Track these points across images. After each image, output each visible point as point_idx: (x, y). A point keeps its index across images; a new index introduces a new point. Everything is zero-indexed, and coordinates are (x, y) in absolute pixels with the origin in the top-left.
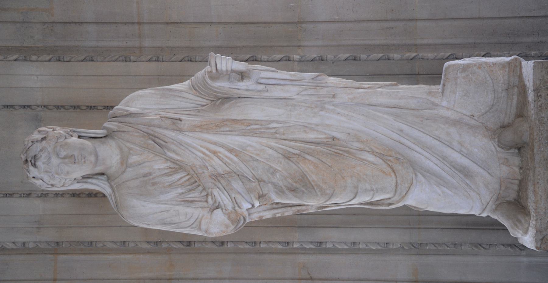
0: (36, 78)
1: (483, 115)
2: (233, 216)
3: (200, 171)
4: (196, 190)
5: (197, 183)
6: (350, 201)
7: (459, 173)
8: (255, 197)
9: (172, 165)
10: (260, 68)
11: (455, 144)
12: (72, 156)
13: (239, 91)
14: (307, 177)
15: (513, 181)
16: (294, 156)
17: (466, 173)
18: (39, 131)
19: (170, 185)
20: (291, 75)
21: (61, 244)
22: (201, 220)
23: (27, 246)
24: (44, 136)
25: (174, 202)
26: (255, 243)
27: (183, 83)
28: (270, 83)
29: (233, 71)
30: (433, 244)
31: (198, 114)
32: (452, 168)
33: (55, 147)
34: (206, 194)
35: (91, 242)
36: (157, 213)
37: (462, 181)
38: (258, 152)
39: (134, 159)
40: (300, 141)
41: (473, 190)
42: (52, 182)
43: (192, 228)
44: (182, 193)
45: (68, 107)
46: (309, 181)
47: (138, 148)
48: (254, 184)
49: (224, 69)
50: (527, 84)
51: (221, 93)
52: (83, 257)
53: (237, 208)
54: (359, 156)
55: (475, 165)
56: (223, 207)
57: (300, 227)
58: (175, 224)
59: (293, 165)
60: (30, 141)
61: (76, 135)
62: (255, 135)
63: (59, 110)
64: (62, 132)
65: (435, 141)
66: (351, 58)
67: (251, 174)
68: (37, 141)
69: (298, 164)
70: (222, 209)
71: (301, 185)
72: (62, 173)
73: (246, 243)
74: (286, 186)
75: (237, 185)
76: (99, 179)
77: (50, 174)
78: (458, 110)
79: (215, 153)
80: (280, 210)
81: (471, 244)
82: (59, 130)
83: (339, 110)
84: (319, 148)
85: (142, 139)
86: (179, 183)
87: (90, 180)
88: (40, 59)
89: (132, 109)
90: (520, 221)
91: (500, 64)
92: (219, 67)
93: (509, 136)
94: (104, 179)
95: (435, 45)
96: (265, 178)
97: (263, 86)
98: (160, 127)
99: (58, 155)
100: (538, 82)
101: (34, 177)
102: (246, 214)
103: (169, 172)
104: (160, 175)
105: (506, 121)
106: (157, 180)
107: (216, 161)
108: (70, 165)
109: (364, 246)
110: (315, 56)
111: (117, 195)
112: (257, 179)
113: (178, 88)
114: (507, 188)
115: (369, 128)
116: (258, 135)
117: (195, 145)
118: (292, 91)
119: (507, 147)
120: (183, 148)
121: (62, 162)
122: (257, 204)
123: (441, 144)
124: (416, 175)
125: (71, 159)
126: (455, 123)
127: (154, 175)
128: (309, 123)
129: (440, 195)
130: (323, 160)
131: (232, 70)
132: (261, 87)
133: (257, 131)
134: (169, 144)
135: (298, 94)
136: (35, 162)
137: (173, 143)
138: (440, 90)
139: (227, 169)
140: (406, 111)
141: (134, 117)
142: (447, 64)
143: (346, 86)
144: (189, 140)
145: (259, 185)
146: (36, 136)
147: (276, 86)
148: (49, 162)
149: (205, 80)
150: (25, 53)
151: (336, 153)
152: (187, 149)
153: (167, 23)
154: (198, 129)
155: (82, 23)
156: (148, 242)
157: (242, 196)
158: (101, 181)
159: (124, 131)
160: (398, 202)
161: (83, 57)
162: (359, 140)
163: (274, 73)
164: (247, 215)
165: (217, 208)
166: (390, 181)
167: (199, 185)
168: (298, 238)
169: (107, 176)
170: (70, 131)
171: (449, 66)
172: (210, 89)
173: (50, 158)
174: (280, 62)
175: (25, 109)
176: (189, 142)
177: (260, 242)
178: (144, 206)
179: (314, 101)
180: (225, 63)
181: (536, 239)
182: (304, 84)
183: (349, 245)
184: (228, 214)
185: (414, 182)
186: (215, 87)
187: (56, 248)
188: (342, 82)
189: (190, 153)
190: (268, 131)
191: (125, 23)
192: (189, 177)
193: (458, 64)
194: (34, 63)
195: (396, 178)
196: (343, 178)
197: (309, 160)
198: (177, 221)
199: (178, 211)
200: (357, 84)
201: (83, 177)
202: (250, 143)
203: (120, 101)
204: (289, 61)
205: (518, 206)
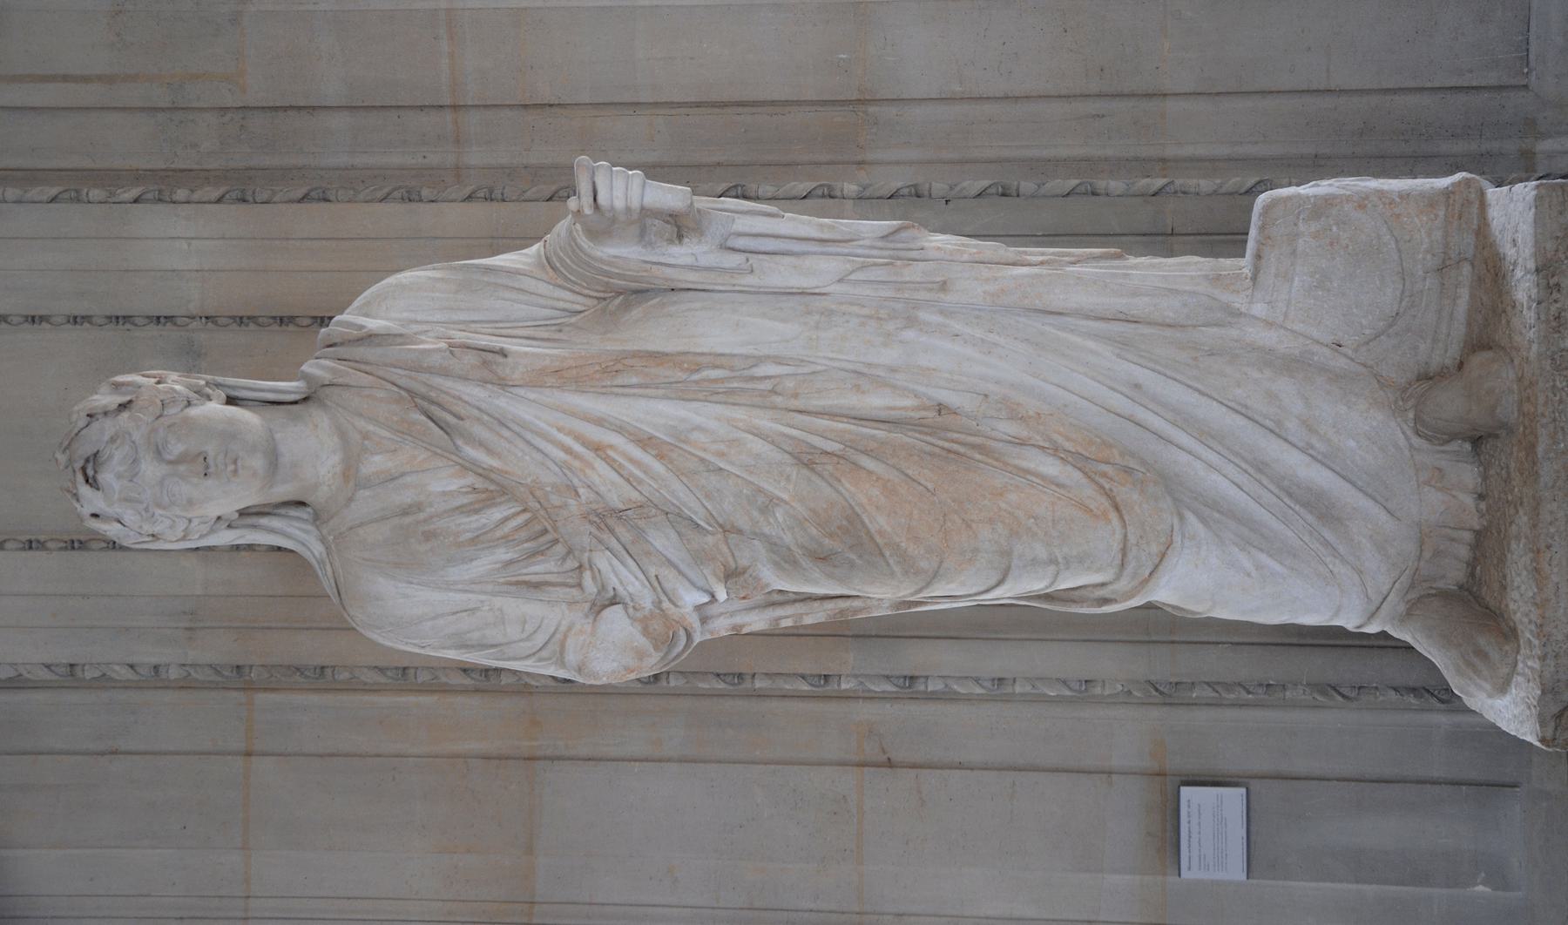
0: (185, 246)
1: (1367, 343)
2: (657, 626)
3: (556, 500)
5: (550, 535)
6: (987, 591)
7: (1302, 511)
8: (715, 575)
9: (480, 483)
11: (1292, 425)
13: (668, 271)
14: (863, 523)
15: (1455, 534)
16: (825, 459)
17: (1321, 508)
19: (473, 540)
20: (821, 226)
22: (565, 637)
25: (490, 587)
26: (740, 676)
28: (763, 249)
29: (646, 212)
30: (1208, 684)
31: (557, 336)
32: (1282, 495)
36: (442, 615)
37: (1311, 534)
38: (722, 447)
39: (376, 463)
41: (1344, 561)
42: (148, 528)
43: (540, 660)
44: (511, 562)
46: (868, 532)
47: (387, 434)
48: (710, 539)
49: (619, 204)
50: (1510, 252)
52: (315, 699)
53: (666, 604)
54: (1016, 462)
55: (1348, 486)
56: (628, 600)
58: (493, 646)
60: (83, 414)
62: (715, 398)
64: (178, 387)
65: (1235, 416)
66: (993, 190)
67: (702, 511)
68: (106, 413)
69: (835, 483)
70: (625, 604)
71: (846, 542)
74: (803, 547)
75: (663, 540)
78: (1298, 327)
79: (598, 449)
80: (789, 610)
81: (1308, 684)
82: (176, 382)
83: (957, 326)
84: (898, 437)
86: (499, 533)
87: (264, 521)
88: (196, 196)
89: (373, 324)
90: (1482, 654)
91: (1422, 195)
93: (1450, 404)
95: (1213, 160)
96: (742, 522)
98: (445, 373)
99: (158, 453)
100: (1550, 245)
101: (95, 515)
102: (694, 620)
105: (1436, 361)
107: (601, 474)
108: (195, 480)
109: (1028, 689)
110: (899, 184)
114: (1437, 553)
115: (1044, 380)
117: (543, 425)
118: (822, 271)
119: (1438, 435)
120: (506, 433)
121: (184, 475)
122: (722, 595)
123: (1250, 424)
124: (1181, 517)
125: (203, 466)
126: (1291, 365)
129: (1249, 575)
130: (910, 472)
131: (643, 208)
132: (734, 260)
133: (720, 387)
134: (467, 424)
135: (840, 281)
138: (1247, 271)
140: (1146, 330)
141: (379, 345)
142: (1262, 199)
143: (977, 258)
144: (525, 413)
146: (105, 399)
147: (778, 258)
149: (574, 240)
150: (161, 185)
151: (949, 451)
152: (518, 435)
153: (525, 106)
154: (551, 380)
155: (314, 108)
156: (465, 670)
157: (680, 572)
160: (1130, 595)
161: (303, 191)
162: (1015, 415)
164: (697, 625)
165: (614, 601)
166: (1106, 537)
167: (556, 541)
168: (849, 663)
170: (208, 384)
171: (1274, 203)
173: (135, 461)
176: (527, 417)
178: (406, 596)
179: (887, 299)
180: (622, 188)
181: (1540, 715)
182: (859, 251)
183: (988, 684)
185: (1177, 538)
186: (601, 261)
187: (238, 677)
188: (967, 246)
190: (750, 386)
191: (422, 108)
192: (527, 516)
193: (1299, 196)
194: (180, 207)
195: (1124, 526)
196: (969, 526)
197: (870, 473)
199: (500, 610)
200: (1011, 252)
201: (243, 513)
202: (698, 420)
203: (349, 303)
205: (1471, 601)
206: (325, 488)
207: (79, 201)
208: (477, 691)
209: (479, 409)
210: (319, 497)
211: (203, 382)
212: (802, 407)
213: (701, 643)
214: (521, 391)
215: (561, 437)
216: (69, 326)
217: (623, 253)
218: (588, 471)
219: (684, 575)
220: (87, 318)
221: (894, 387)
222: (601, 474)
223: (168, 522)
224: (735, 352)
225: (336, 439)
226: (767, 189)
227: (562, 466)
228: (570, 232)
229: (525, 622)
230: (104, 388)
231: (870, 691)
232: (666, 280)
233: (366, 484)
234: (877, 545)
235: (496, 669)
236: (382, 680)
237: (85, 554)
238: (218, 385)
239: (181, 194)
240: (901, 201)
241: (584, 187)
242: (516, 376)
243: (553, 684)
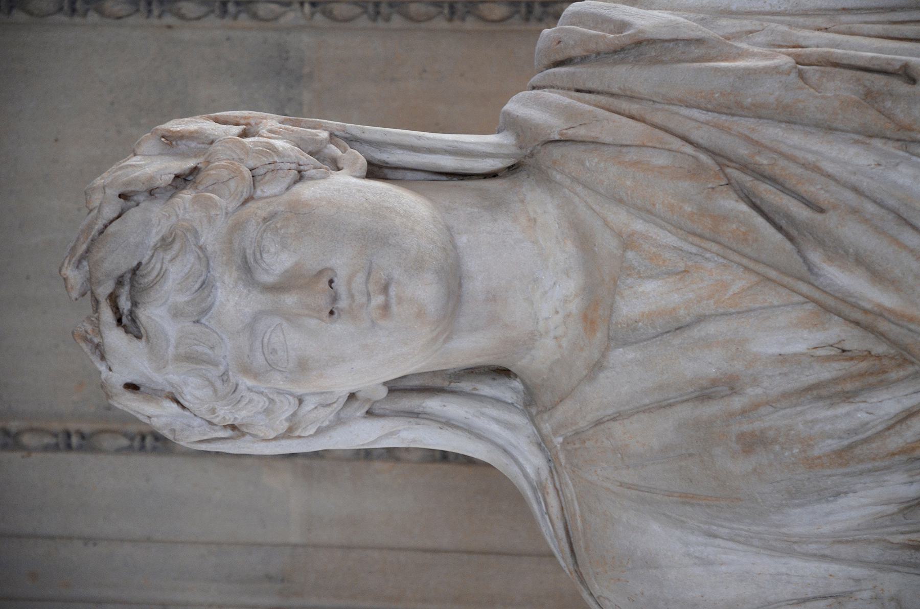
9: (855, 341)
12: (321, 273)
18: (171, 141)
24: (191, 163)
33: (238, 227)
42: (225, 414)
47: (670, 239)
60: (113, 193)
61: (358, 158)
63: (381, 24)
64: (279, 144)
68: (152, 193)
72: (272, 367)
76: (482, 398)
77: (214, 373)
82: (276, 135)
85: (685, 185)
86: (895, 442)
87: (433, 404)
98: (789, 117)
99: (247, 270)
101: (132, 387)
103: (835, 381)
104: (785, 395)
106: (770, 421)
108: (313, 323)
111: (570, 492)
125: (324, 294)
127: (753, 392)
134: (831, 221)
136: (135, 304)
141: (656, 61)
146: (150, 165)
148: (200, 310)
159: (595, 143)
169: (523, 383)
170: (333, 137)
173: (206, 285)
201: (395, 388)
206: (549, 342)
209: (855, 190)
210: (538, 360)
211: (324, 135)
216: (62, 18)
223: (262, 403)
230: (149, 144)
237: (90, 458)
238: (352, 141)
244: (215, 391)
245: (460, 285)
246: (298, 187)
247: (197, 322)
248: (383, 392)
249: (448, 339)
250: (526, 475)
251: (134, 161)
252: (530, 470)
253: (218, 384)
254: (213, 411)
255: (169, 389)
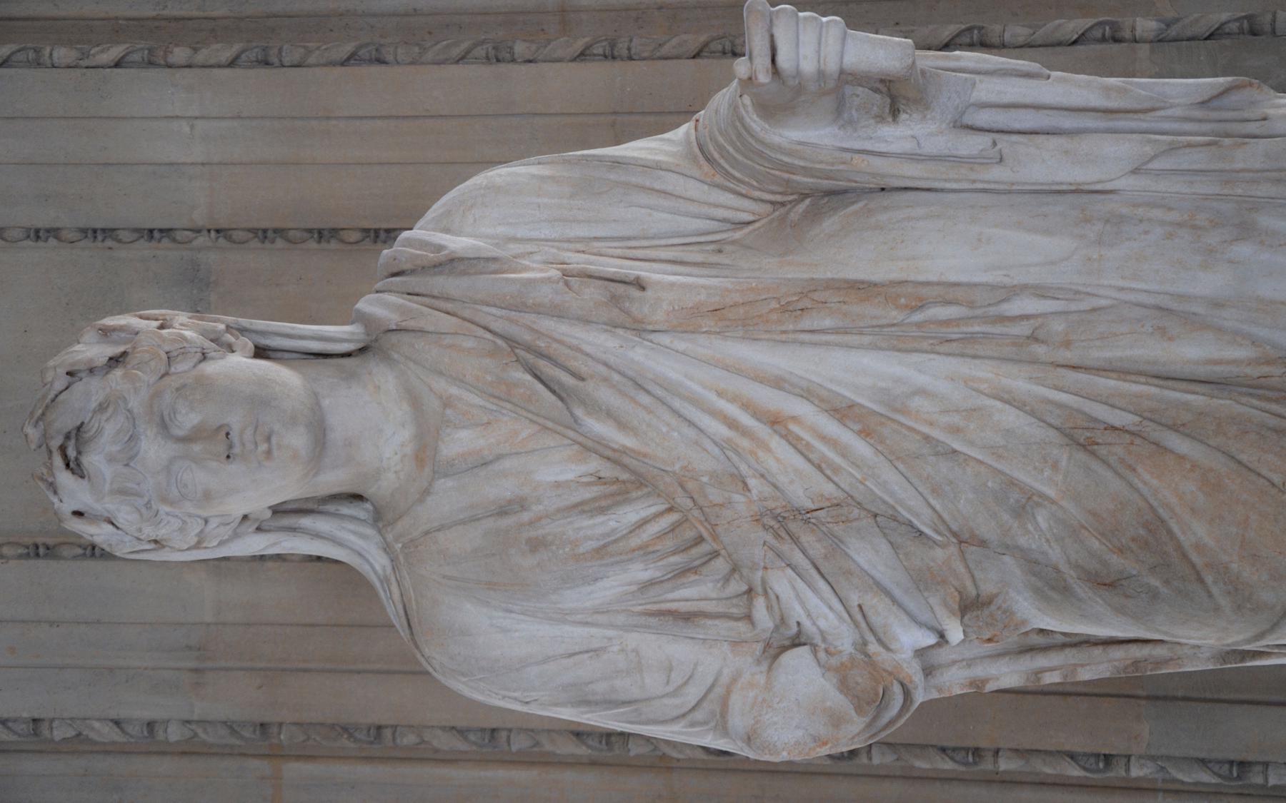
0: (187, 129)
2: (860, 678)
3: (715, 495)
4: (705, 570)
8: (945, 604)
9: (608, 471)
10: (971, 65)
12: (220, 427)
13: (877, 162)
16: (1110, 437)
18: (106, 332)
20: (1107, 89)
21: (275, 730)
22: (728, 692)
23: (160, 735)
24: (121, 349)
25: (620, 619)
26: (977, 752)
27: (666, 136)
28: (1017, 126)
29: (847, 78)
33: (157, 395)
34: (745, 588)
35: (379, 728)
38: (956, 419)
39: (460, 442)
40: (1140, 373)
42: (149, 531)
43: (692, 725)
44: (651, 583)
45: (298, 234)
46: (1179, 547)
47: (478, 400)
48: (939, 553)
49: (808, 67)
51: (806, 171)
52: (365, 771)
53: (874, 647)
56: (818, 640)
57: (1157, 698)
58: (629, 703)
59: (1109, 474)
60: (62, 371)
63: (267, 245)
67: (927, 512)
68: (91, 371)
73: (943, 750)
74: (1077, 567)
75: (870, 554)
76: (342, 517)
79: (776, 422)
80: (1055, 659)
82: (186, 327)
86: (635, 541)
87: (306, 522)
88: (200, 57)
89: (457, 243)
92: (784, 60)
94: (362, 515)
96: (986, 529)
97: (986, 140)
98: (559, 313)
99: (164, 426)
101: (78, 514)
103: (595, 499)
104: (558, 510)
107: (781, 458)
108: (214, 464)
110: (1224, 16)
111: (407, 583)
112: (955, 534)
113: (635, 154)
116: (954, 347)
120: (645, 399)
122: (955, 633)
125: (220, 442)
127: (537, 509)
128: (1181, 297)
130: (1244, 457)
131: (842, 72)
132: (974, 144)
133: (953, 332)
134: (590, 386)
136: (79, 453)
137: (606, 380)
139: (829, 489)
141: (464, 273)
145: (964, 559)
146: (91, 350)
148: (128, 455)
149: (741, 120)
157: (894, 601)
158: (351, 526)
159: (422, 331)
161: (349, 48)
163: (1033, 83)
164: (918, 678)
165: (796, 642)
167: (715, 554)
170: (229, 328)
172: (760, 154)
174: (1079, 47)
175: (154, 244)
177: (997, 752)
179: (1206, 197)
180: (816, 44)
182: (1166, 126)
184: (837, 670)
186: (779, 149)
189: (674, 421)
190: (998, 329)
192: (674, 517)
194: (179, 74)
197: (1182, 458)
198: (636, 693)
199: (636, 651)
201: (278, 511)
202: (922, 380)
204: (1116, 40)
207: (39, 64)
208: (593, 763)
209: (606, 364)
211: (222, 327)
212: (1075, 361)
213: (922, 704)
214: (665, 339)
215: (723, 405)
217: (812, 137)
218: (761, 454)
219: (900, 606)
220: (54, 232)
221: (1219, 330)
222: (781, 458)
223: (176, 524)
224: (976, 279)
225: (405, 407)
226: (1018, 32)
227: (724, 446)
228: (734, 108)
229: (671, 669)
230: (90, 335)
231: (1175, 781)
232: (874, 175)
233: (448, 470)
234: (1193, 566)
235: (622, 734)
236: (461, 745)
237: (53, 564)
238: (243, 331)
239: (180, 54)
240: (1227, 42)
241: (758, 43)
242: (659, 316)
243: (704, 756)
244: (141, 515)
245: (325, 435)
246: (202, 365)
247: (127, 465)
248: (269, 514)
249: (316, 474)
250: (375, 572)
251: (77, 347)
252: (378, 568)
253: (143, 510)
254: (140, 530)
255: (106, 514)
